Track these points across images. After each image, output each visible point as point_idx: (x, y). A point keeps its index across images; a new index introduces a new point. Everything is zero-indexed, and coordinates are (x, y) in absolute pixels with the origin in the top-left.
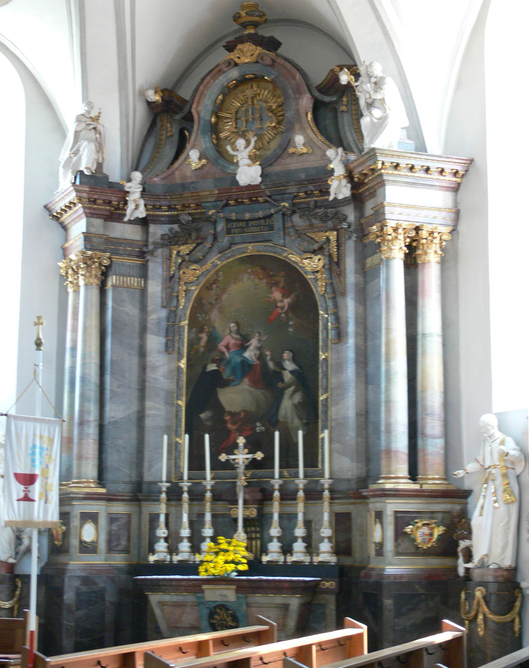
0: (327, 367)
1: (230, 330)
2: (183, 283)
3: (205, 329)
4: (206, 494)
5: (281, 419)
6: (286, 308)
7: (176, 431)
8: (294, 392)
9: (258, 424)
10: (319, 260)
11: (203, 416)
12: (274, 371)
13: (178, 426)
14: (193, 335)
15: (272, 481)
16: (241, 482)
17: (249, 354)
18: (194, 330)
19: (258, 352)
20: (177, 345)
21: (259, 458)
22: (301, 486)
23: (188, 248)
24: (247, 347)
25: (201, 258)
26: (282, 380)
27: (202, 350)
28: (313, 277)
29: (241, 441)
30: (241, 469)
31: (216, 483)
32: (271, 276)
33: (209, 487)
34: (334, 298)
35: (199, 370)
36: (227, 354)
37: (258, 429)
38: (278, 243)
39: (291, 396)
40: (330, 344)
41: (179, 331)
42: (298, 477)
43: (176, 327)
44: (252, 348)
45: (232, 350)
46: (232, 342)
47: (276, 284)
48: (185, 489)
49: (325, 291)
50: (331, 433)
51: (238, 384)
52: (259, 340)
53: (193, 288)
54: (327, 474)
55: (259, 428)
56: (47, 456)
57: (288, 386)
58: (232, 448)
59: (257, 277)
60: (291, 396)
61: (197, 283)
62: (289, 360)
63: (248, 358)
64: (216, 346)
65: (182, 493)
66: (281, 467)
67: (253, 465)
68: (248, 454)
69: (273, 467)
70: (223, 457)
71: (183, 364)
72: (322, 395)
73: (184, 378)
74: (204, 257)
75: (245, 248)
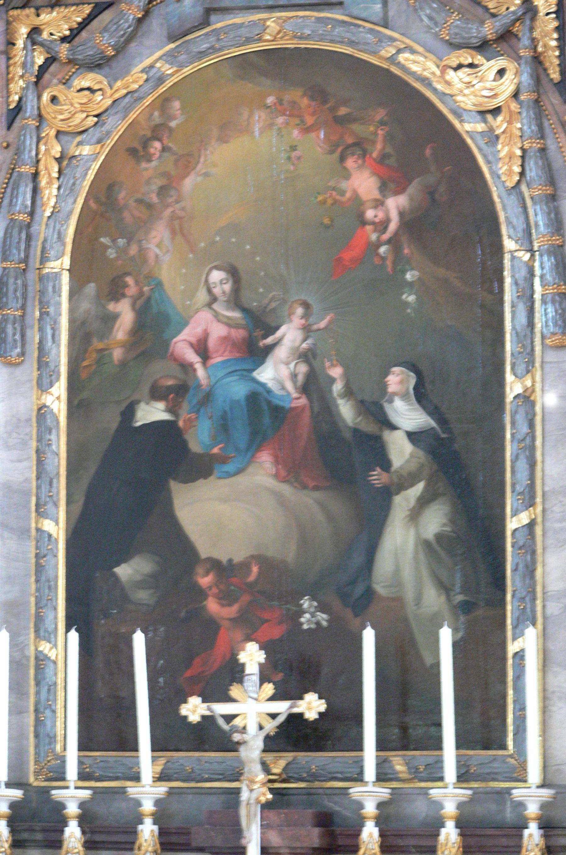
0: (531, 425)
1: (209, 291)
2: (53, 133)
3: (126, 286)
4: (140, 827)
5: (380, 589)
6: (393, 227)
7: (39, 619)
8: (424, 502)
9: (306, 603)
10: (501, 72)
11: (124, 571)
12: (356, 431)
13: (43, 602)
14: (85, 305)
15: (356, 791)
16: (254, 791)
17: (276, 374)
18: (91, 289)
19: (303, 369)
20: (34, 337)
21: (311, 715)
22: (450, 808)
23: (67, 18)
24: (269, 349)
25: (110, 52)
26: (385, 463)
27: (117, 354)
28: (480, 127)
29: (252, 656)
30: (253, 750)
31: (171, 792)
32: (340, 121)
33: (148, 806)
34: (553, 198)
35: (111, 420)
36: (201, 372)
37: (306, 621)
38: (363, 15)
39: (415, 515)
40: (538, 348)
41: (42, 293)
42: (441, 779)
43: (32, 276)
44: (281, 352)
45: (217, 360)
46: (218, 331)
47: (360, 147)
48: (72, 809)
49: (522, 174)
50: (545, 635)
51: (239, 471)
52: (307, 330)
53: (86, 150)
54: (534, 773)
55: (311, 616)
56: (39, 293)
57: (403, 484)
58: (222, 680)
59: (297, 121)
60: (415, 515)
61: (97, 133)
62: (404, 396)
63: (271, 385)
64: (166, 344)
65: (63, 822)
66: (382, 745)
67: (292, 735)
68: (272, 699)
69: (357, 745)
70: (194, 709)
71: (57, 400)
72: (515, 513)
73: (60, 444)
74: (120, 49)
75: (254, 24)
